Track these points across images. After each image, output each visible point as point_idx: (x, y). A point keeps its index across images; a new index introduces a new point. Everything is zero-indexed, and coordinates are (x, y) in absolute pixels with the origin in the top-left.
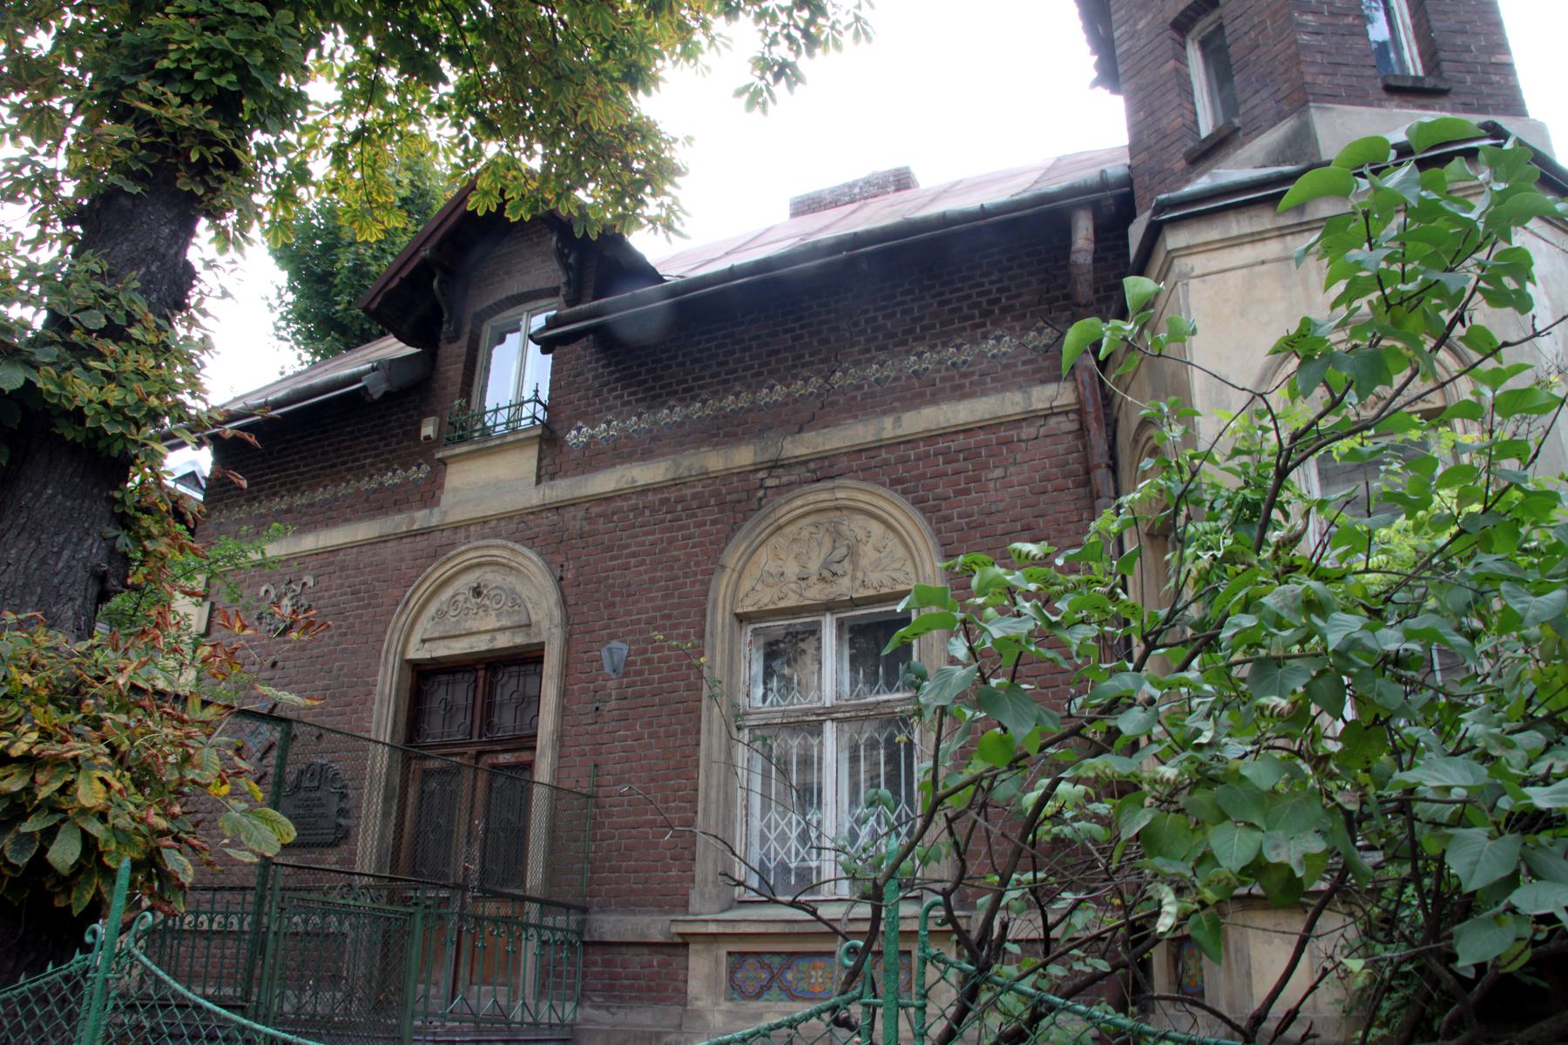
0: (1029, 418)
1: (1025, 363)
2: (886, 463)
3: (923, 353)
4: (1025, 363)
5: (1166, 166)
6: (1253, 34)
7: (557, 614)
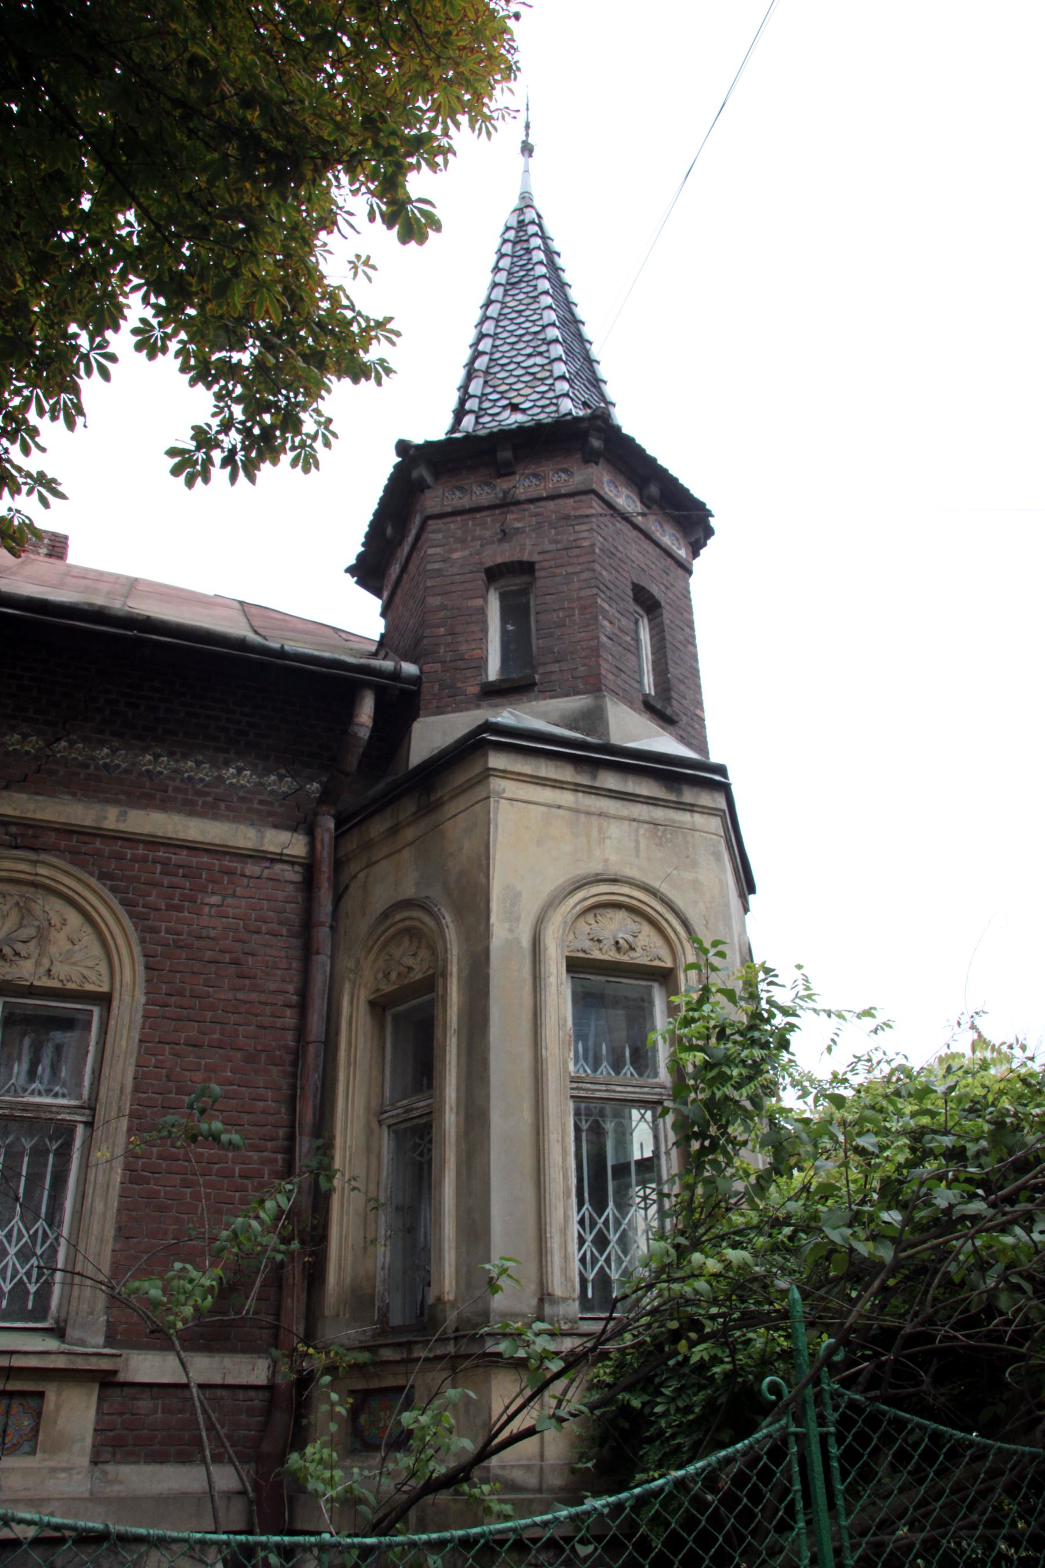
0: (259, 856)
1: (261, 802)
2: (99, 853)
3: (29, 735)
4: (261, 802)
5: (459, 685)
6: (561, 614)
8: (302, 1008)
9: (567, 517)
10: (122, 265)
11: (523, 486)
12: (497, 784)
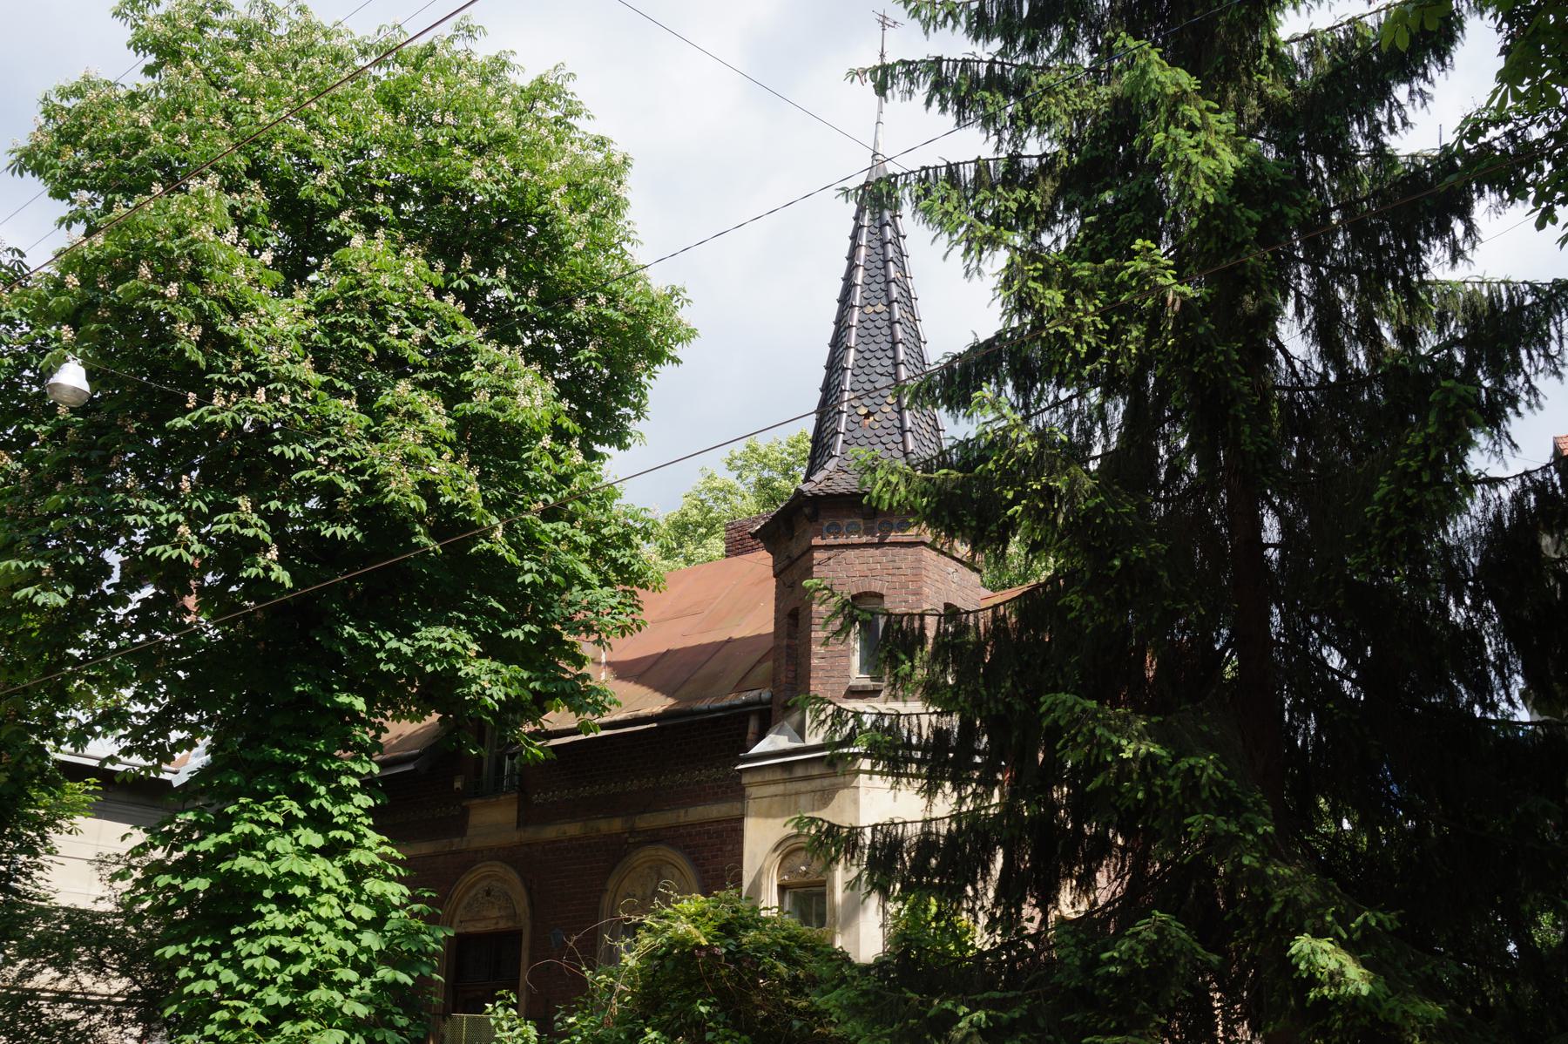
7: (528, 910)
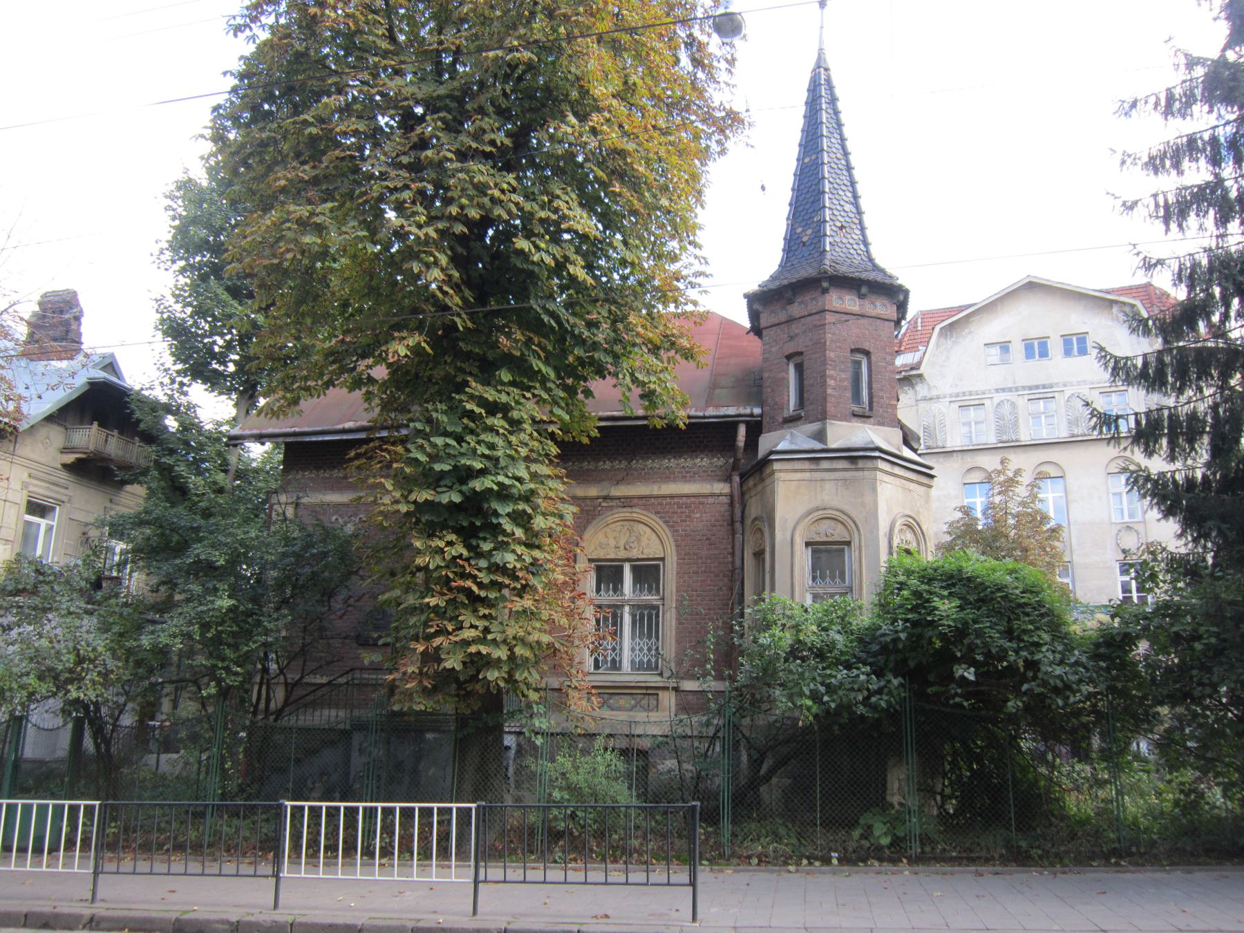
0: (713, 495)
8: (733, 554)
9: (816, 326)
10: (430, 351)
11: (796, 310)
12: (777, 475)
